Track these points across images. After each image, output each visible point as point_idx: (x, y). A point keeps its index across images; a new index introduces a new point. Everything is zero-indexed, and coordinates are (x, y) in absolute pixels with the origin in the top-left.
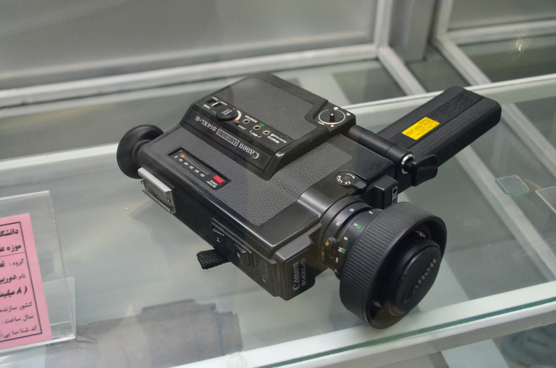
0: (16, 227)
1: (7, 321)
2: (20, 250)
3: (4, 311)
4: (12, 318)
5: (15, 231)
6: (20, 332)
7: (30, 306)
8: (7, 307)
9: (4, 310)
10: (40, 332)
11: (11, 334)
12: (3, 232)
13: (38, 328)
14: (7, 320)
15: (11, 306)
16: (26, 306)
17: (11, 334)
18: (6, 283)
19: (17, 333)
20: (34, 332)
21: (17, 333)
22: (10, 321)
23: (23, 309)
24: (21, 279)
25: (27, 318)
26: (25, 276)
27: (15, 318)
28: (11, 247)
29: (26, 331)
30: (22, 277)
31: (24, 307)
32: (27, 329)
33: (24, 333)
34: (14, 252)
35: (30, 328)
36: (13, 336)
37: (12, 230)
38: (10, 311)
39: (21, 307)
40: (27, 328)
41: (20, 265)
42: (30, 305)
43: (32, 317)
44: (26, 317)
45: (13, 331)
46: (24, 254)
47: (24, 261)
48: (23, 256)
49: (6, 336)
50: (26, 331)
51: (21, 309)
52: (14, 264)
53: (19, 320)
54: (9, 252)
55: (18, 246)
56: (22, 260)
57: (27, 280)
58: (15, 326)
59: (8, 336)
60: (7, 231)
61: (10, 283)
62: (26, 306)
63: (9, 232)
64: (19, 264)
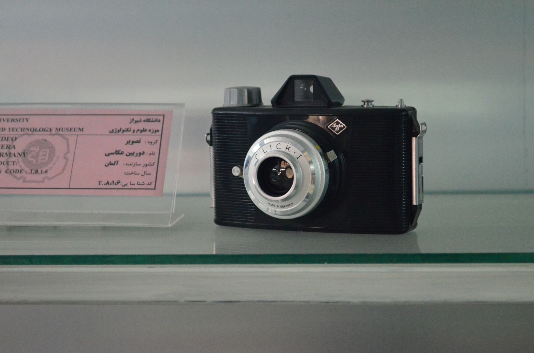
0: (161, 118)
1: (127, 173)
2: (157, 133)
3: (129, 165)
4: (132, 172)
5: (158, 120)
6: (136, 184)
7: (153, 165)
8: (132, 163)
9: (129, 164)
10: (154, 188)
11: (129, 184)
12: (150, 119)
13: (153, 184)
14: (127, 172)
15: (136, 163)
16: (149, 165)
17: (129, 184)
18: (136, 156)
19: (134, 184)
20: (149, 187)
21: (134, 184)
22: (129, 174)
23: (146, 166)
24: (150, 155)
25: (144, 174)
26: (154, 154)
27: (135, 172)
28: (152, 130)
29: (142, 184)
30: (152, 155)
31: (147, 165)
32: (143, 183)
33: (140, 186)
34: (153, 134)
35: (146, 183)
36: (129, 186)
37: (156, 119)
38: (134, 166)
39: (144, 165)
40: (143, 182)
41: (154, 144)
42: (152, 164)
43: (150, 174)
44: (144, 173)
45: (131, 182)
46: (160, 136)
47: (157, 142)
48: (159, 138)
49: (123, 185)
50: (142, 184)
51: (143, 166)
52: (149, 142)
53: (139, 165)
54: (150, 133)
55: (157, 130)
56: (157, 141)
57: (154, 159)
58: (135, 179)
59: (125, 185)
60: (153, 119)
61: (139, 157)
62: (149, 165)
63: (154, 120)
64: (153, 143)
